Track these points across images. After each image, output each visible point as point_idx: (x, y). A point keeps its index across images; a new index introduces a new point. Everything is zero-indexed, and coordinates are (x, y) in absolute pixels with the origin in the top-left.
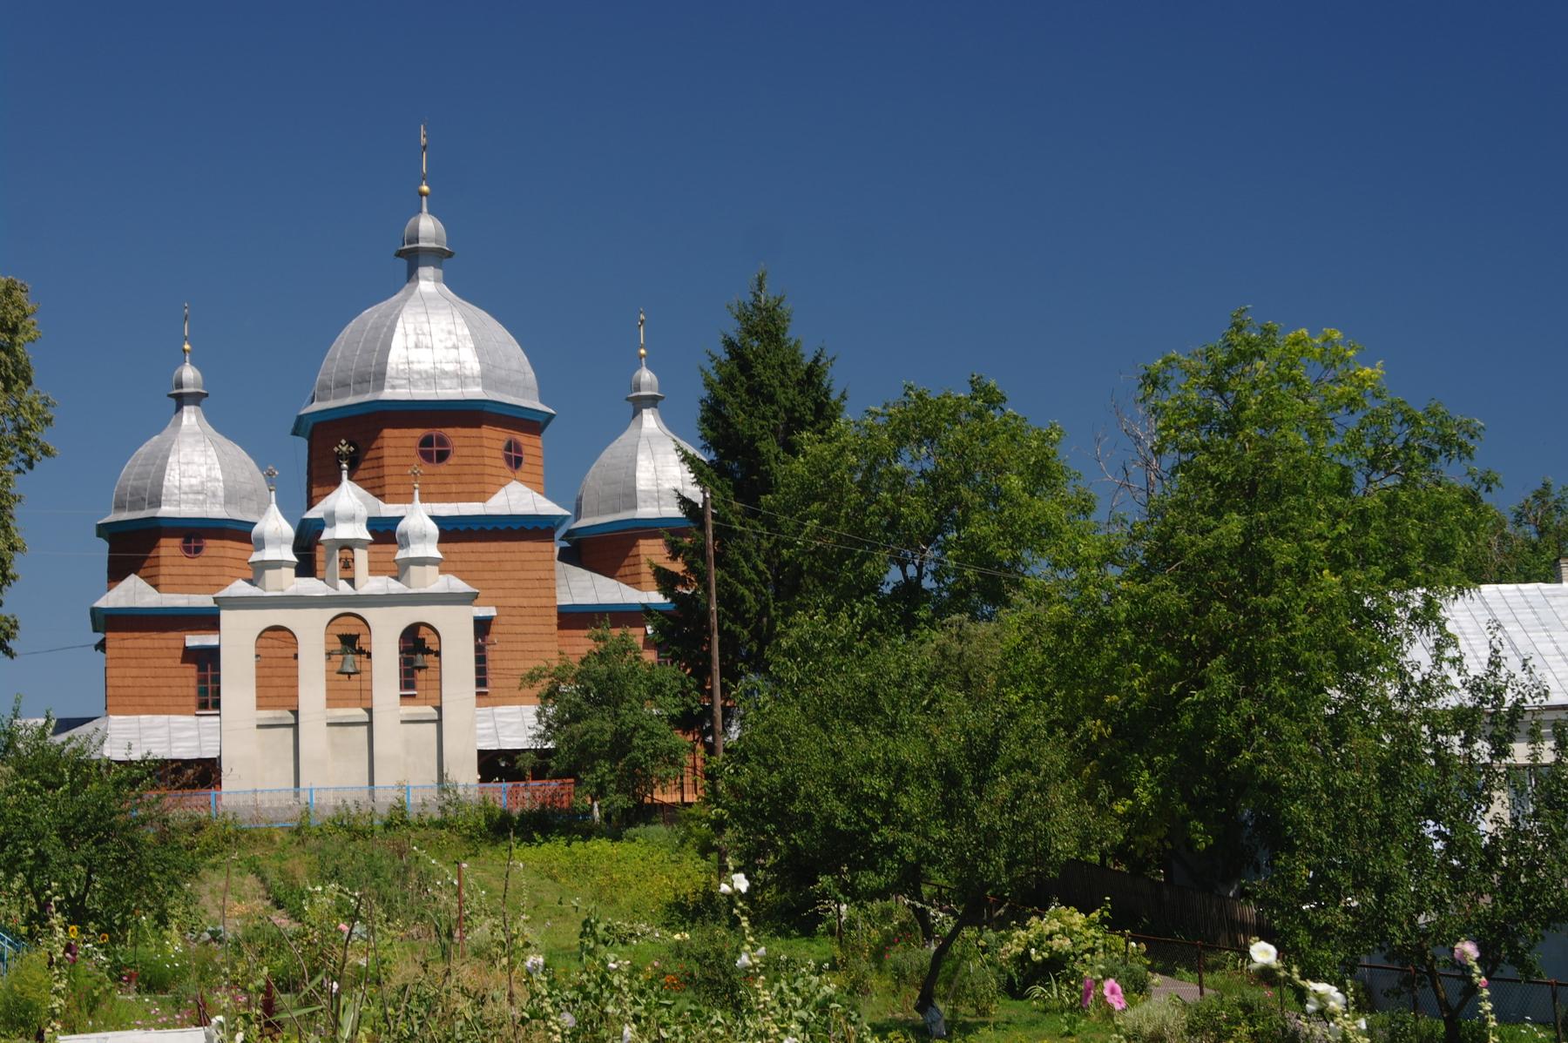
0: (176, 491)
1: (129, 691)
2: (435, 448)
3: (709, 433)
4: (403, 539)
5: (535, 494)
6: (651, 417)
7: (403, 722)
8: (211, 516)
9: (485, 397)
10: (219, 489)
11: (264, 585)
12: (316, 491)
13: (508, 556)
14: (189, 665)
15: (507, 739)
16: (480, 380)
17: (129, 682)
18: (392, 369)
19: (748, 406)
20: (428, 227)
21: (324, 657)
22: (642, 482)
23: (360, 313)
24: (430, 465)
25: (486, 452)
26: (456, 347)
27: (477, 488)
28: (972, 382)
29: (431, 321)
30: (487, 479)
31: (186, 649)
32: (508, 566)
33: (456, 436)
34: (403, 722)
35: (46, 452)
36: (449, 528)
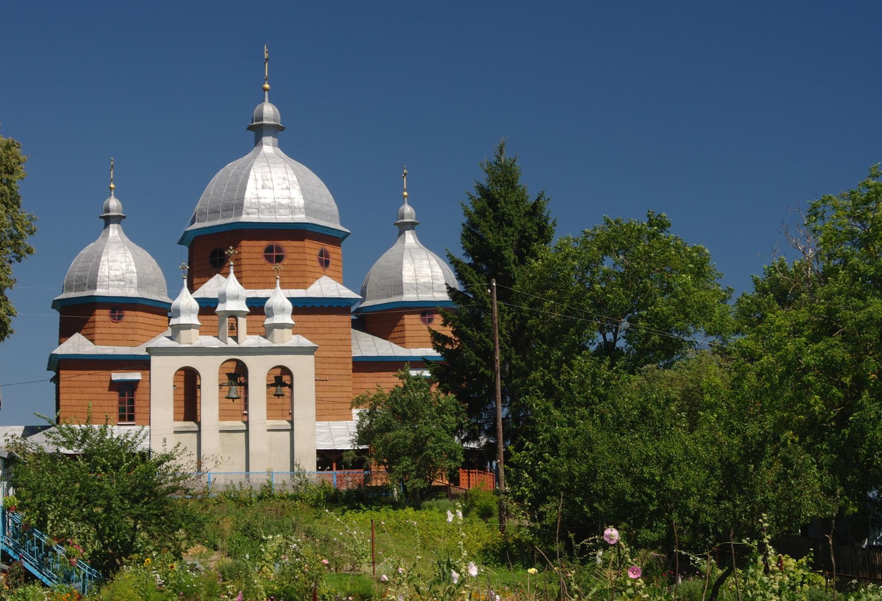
0: (107, 279)
1: (75, 409)
2: (275, 254)
3: (468, 245)
4: (269, 311)
5: (338, 284)
6: (411, 236)
7: (268, 430)
8: (129, 296)
9: (307, 221)
10: (134, 278)
11: (180, 339)
12: (196, 281)
13: (321, 324)
14: (114, 392)
15: (321, 443)
16: (304, 210)
17: (74, 403)
18: (247, 202)
19: (495, 228)
20: (269, 111)
21: (217, 387)
22: (406, 278)
23: (225, 165)
24: (271, 264)
25: (308, 257)
26: (288, 188)
27: (301, 280)
28: (649, 216)
29: (272, 171)
30: (308, 274)
31: (112, 381)
32: (321, 330)
33: (287, 246)
34: (268, 430)
35: (29, 251)
36: (300, 306)
